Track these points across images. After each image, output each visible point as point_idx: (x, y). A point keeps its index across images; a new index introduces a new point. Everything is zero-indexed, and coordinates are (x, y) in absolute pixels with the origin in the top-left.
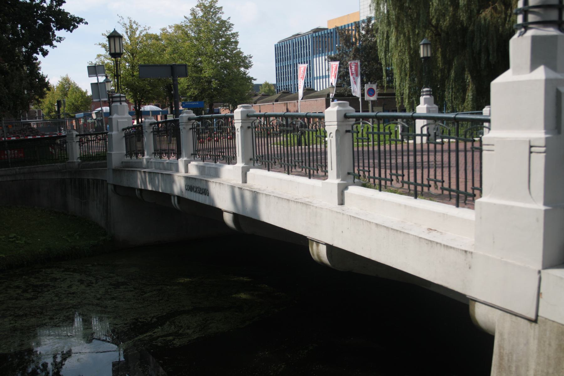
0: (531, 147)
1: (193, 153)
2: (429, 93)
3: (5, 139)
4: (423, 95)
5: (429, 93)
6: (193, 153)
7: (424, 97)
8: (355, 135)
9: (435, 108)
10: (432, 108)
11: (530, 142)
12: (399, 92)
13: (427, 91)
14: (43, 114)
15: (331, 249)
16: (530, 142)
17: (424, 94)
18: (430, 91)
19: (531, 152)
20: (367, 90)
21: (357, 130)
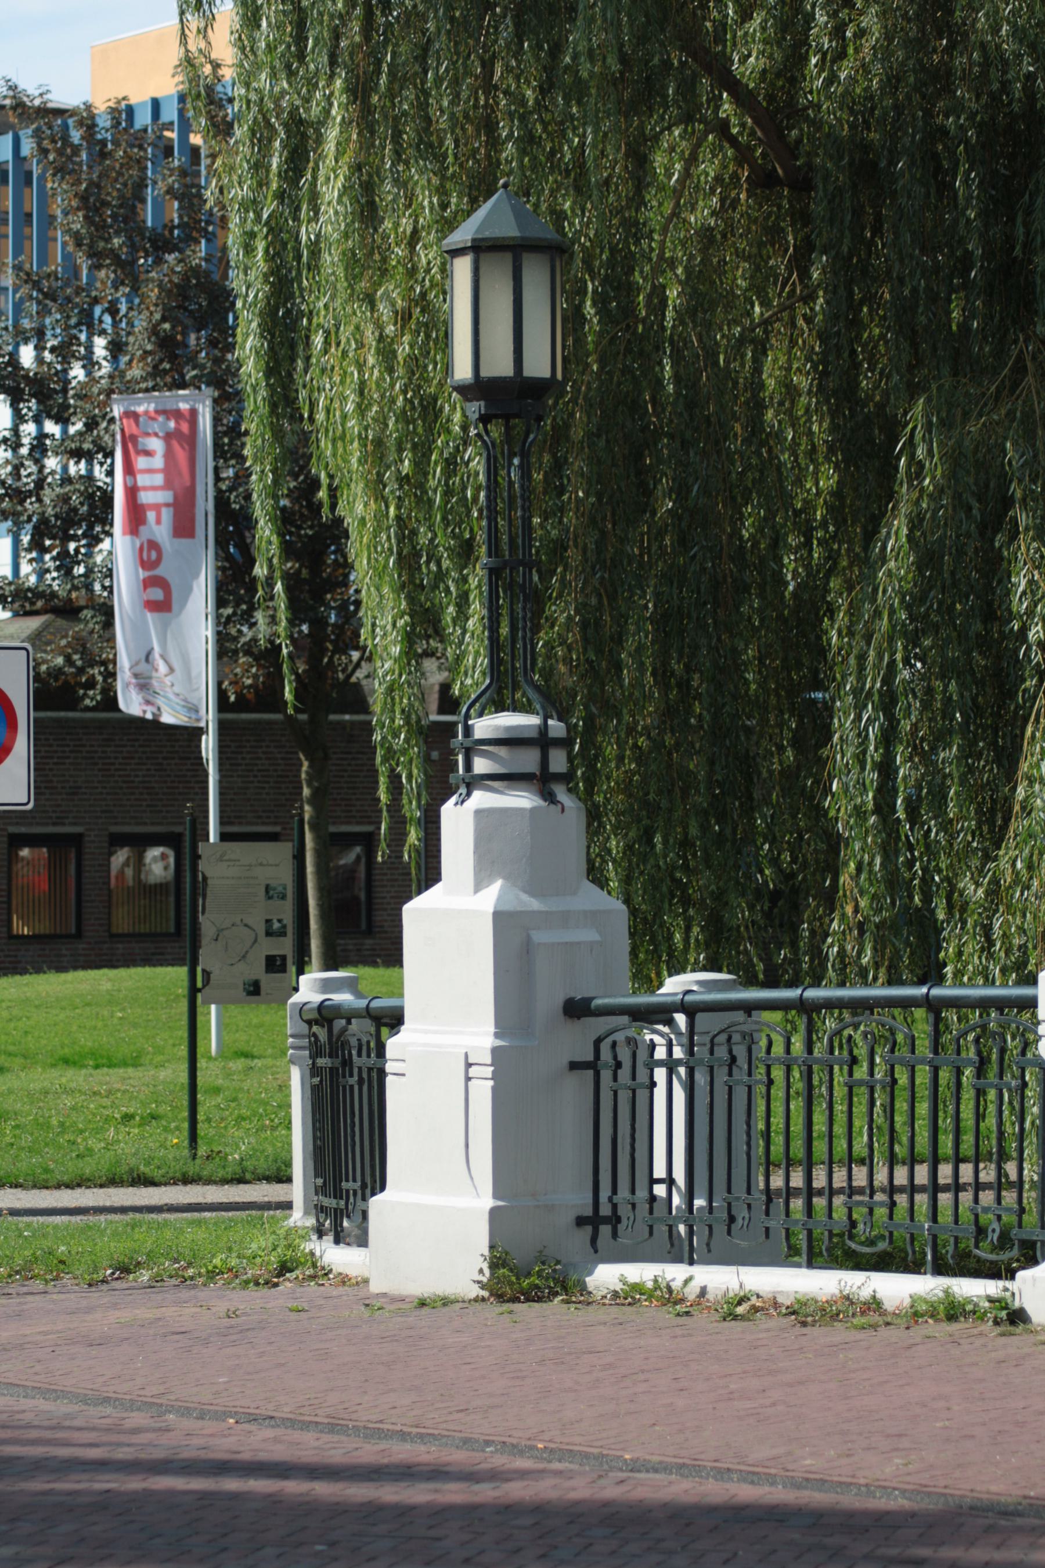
0: (469, 1065)
1: (589, 1212)
2: (528, 760)
3: (740, 133)
4: (473, 783)
5: (528, 760)
6: (589, 1212)
7: (480, 799)
8: (606, 1075)
9: (593, 917)
10: (565, 919)
11: (466, 1056)
12: (399, 722)
13: (511, 741)
14: (962, 1525)
15: (316, 1177)
16: (466, 1056)
17: (481, 765)
18: (542, 741)
19: (468, 1079)
20: (190, 606)
21: (615, 1057)
